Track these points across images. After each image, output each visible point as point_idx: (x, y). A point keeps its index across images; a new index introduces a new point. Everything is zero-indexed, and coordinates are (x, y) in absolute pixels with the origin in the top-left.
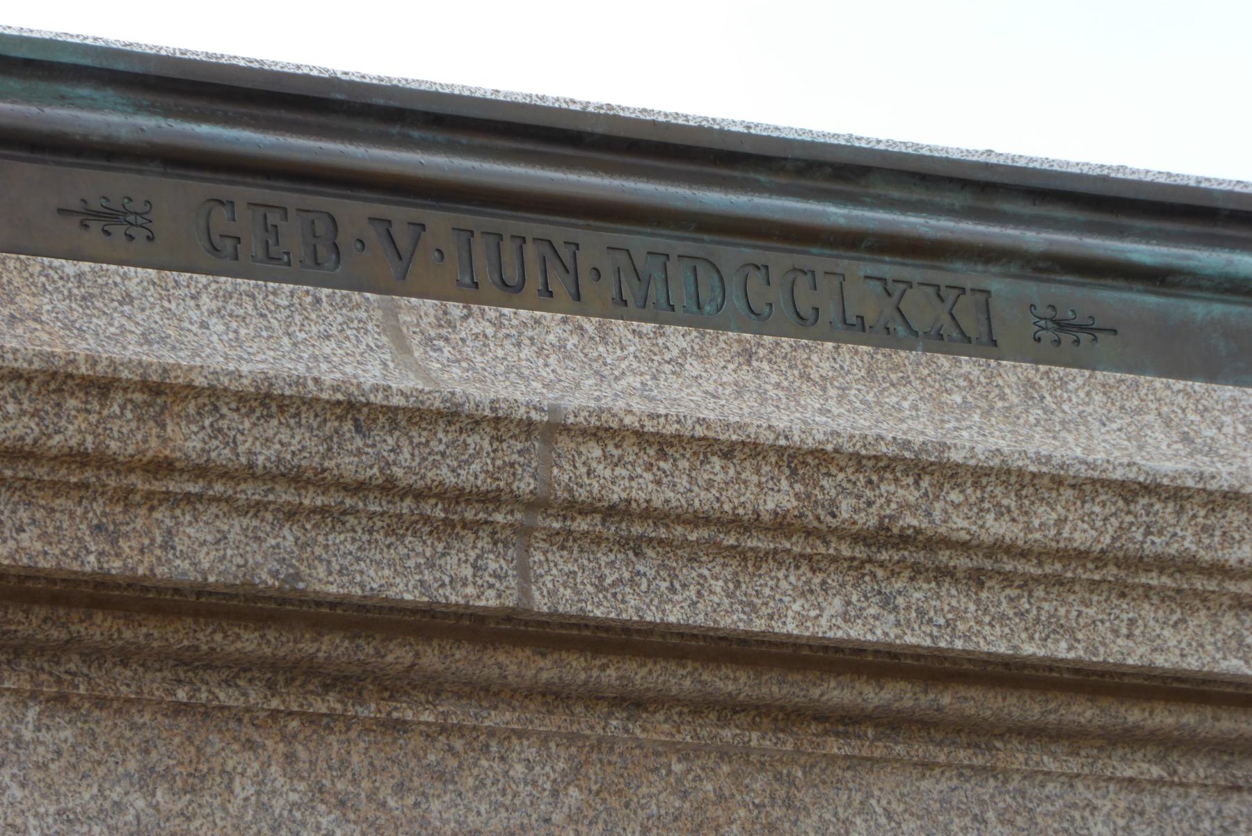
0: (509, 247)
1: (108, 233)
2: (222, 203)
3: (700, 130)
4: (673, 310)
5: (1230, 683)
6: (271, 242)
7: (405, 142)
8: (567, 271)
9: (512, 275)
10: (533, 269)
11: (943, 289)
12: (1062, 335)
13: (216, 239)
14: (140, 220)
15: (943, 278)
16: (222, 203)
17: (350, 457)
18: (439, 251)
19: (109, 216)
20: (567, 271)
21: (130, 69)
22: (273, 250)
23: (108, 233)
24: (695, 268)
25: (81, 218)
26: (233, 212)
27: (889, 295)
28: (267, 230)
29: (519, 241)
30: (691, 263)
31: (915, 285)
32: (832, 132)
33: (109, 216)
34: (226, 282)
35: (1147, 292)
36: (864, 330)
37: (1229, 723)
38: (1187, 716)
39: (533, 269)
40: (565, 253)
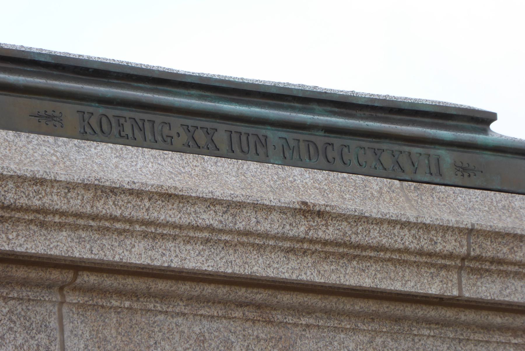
0: (235, 137)
1: (47, 124)
2: (330, 144)
3: (163, 72)
4: (233, 152)
5: (515, 306)
6: (121, 130)
7: (293, 109)
8: (141, 130)
9: (245, 149)
10: (252, 145)
11: (376, 150)
12: (465, 173)
13: (165, 137)
14: (58, 120)
15: (376, 146)
16: (330, 144)
17: (103, 207)
18: (274, 146)
19: (49, 117)
20: (141, 130)
21: (46, 60)
22: (123, 134)
23: (47, 124)
24: (308, 145)
25: (38, 118)
26: (333, 148)
27: (208, 134)
28: (119, 126)
29: (229, 133)
30: (307, 143)
31: (199, 128)
32: (342, 90)
33: (49, 117)
34: (154, 152)
35: (405, 145)
36: (128, 139)
37: (520, 321)
38: (33, 276)
39: (252, 145)
40: (140, 124)
